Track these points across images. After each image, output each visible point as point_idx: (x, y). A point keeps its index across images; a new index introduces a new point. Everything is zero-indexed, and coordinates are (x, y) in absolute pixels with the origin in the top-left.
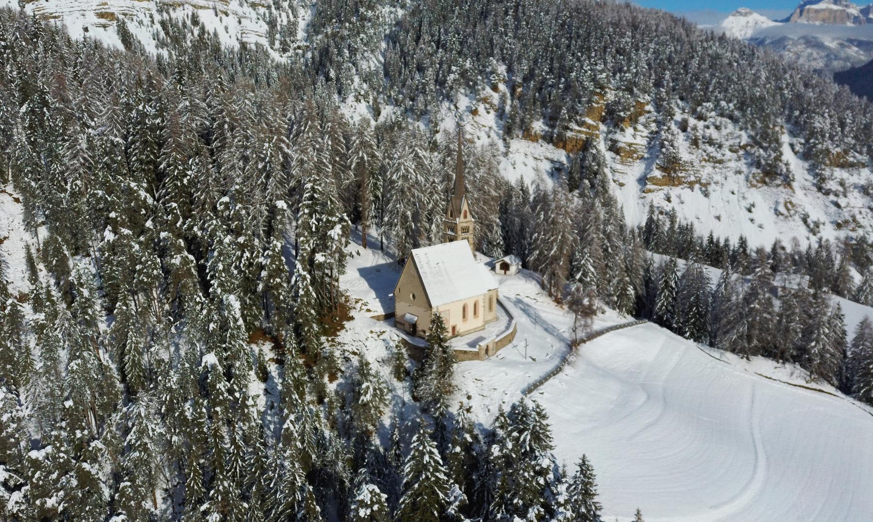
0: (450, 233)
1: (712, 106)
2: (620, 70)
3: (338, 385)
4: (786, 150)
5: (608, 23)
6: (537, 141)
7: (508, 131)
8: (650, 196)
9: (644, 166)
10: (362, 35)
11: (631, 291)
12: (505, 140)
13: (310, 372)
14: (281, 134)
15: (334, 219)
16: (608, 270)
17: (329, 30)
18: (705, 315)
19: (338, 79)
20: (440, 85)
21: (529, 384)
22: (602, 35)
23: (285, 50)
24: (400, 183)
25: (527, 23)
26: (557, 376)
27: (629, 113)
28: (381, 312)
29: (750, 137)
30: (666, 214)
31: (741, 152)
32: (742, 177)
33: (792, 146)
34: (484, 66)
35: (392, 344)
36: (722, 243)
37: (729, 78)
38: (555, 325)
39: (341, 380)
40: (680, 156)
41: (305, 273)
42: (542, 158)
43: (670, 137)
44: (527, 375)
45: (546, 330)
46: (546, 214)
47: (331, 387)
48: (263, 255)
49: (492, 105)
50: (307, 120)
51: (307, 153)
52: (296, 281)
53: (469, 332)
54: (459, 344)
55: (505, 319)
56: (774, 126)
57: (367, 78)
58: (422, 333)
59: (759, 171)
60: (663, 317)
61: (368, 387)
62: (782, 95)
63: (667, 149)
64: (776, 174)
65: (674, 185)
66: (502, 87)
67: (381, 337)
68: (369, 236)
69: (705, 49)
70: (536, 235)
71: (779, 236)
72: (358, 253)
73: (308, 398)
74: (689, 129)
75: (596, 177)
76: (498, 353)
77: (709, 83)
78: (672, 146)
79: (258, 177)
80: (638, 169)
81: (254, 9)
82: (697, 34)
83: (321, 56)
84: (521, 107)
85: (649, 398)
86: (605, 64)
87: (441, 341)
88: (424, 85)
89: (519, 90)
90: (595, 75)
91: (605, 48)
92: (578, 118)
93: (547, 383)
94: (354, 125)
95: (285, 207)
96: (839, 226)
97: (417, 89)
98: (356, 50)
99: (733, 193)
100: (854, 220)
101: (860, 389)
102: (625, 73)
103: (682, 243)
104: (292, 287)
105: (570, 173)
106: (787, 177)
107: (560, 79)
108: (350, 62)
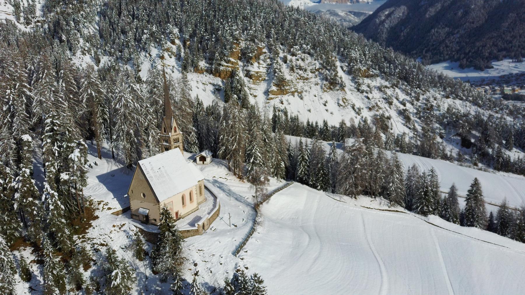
0: (165, 144)
2: (246, 29)
3: (92, 272)
4: (339, 69)
6: (203, 73)
7: (185, 68)
10: (82, 12)
13: (67, 266)
14: (23, 81)
15: (73, 145)
17: (59, 10)
18: (328, 174)
19: (68, 41)
20: (138, 42)
21: (236, 246)
22: (234, 9)
23: (28, 24)
24: (122, 110)
25: (188, 3)
27: (254, 54)
28: (119, 208)
31: (317, 73)
32: (319, 87)
33: (342, 67)
34: (164, 29)
35: (131, 233)
36: (314, 124)
38: (241, 195)
39: (94, 268)
41: (53, 192)
42: (207, 83)
44: (234, 239)
45: (236, 199)
47: (86, 275)
48: (14, 180)
49: (172, 53)
50: (44, 69)
51: (45, 95)
52: (46, 199)
55: (212, 198)
56: (332, 57)
57: (88, 39)
58: (154, 221)
59: (327, 83)
61: (117, 274)
62: (334, 40)
64: (336, 83)
65: (284, 94)
66: (177, 41)
67: (122, 229)
68: (103, 148)
69: (290, 16)
70: (222, 136)
71: (343, 118)
72: (96, 164)
73: (68, 287)
74: (288, 62)
75: (240, 93)
78: (280, 71)
79: (4, 117)
80: (263, 86)
82: (285, 7)
83: (55, 26)
85: (310, 238)
86: (237, 25)
88: (127, 42)
89: (188, 43)
90: (232, 33)
91: (236, 16)
94: (83, 70)
95: (30, 139)
96: (370, 109)
97: (123, 45)
98: (79, 22)
99: (315, 96)
100: (377, 106)
101: (417, 207)
102: (249, 31)
103: (295, 128)
104: (43, 203)
105: (226, 91)
106: (342, 85)
107: (212, 36)
108: (76, 30)
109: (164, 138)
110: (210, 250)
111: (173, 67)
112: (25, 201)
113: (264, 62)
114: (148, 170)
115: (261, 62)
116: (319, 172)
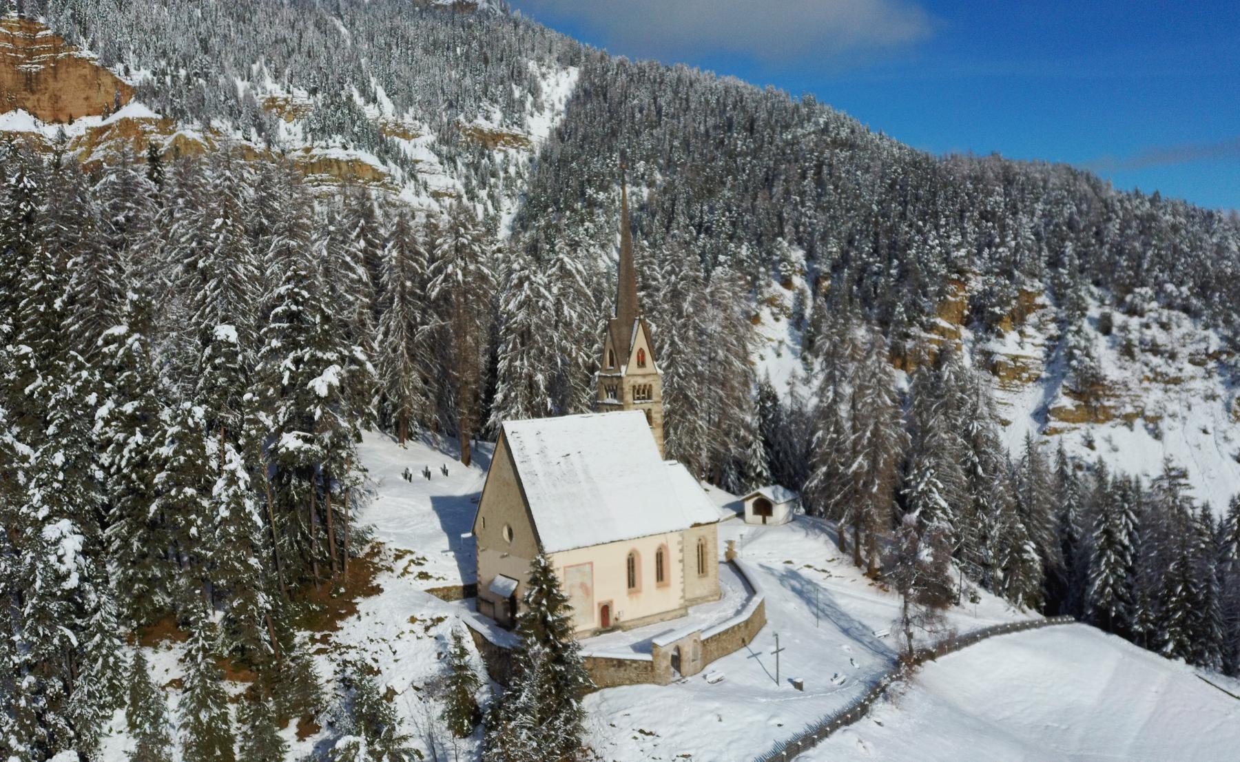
1: (1150, 292)
5: (964, 178)
10: (587, 224)
12: (804, 359)
16: (980, 514)
18: (1208, 600)
21: (777, 744)
22: (956, 194)
27: (1009, 308)
28: (454, 578)
29: (1223, 338)
31: (1212, 365)
32: (1218, 406)
37: (1175, 247)
38: (866, 622)
40: (1103, 373)
43: (1083, 343)
44: (776, 721)
45: (846, 631)
49: (782, 308)
60: (1108, 611)
63: (1080, 362)
65: (1097, 421)
66: (798, 281)
67: (433, 631)
72: (445, 472)
74: (1114, 331)
76: (710, 667)
77: (1141, 257)
78: (1088, 355)
81: (437, 201)
84: (830, 308)
86: (964, 235)
89: (826, 283)
90: (948, 253)
91: (962, 211)
92: (924, 319)
93: (827, 742)
99: (1205, 432)
102: (998, 246)
107: (890, 261)
109: (607, 382)
110: (678, 739)
111: (781, 342)
112: (173, 493)
113: (1039, 329)
114: (526, 452)
116: (1171, 591)
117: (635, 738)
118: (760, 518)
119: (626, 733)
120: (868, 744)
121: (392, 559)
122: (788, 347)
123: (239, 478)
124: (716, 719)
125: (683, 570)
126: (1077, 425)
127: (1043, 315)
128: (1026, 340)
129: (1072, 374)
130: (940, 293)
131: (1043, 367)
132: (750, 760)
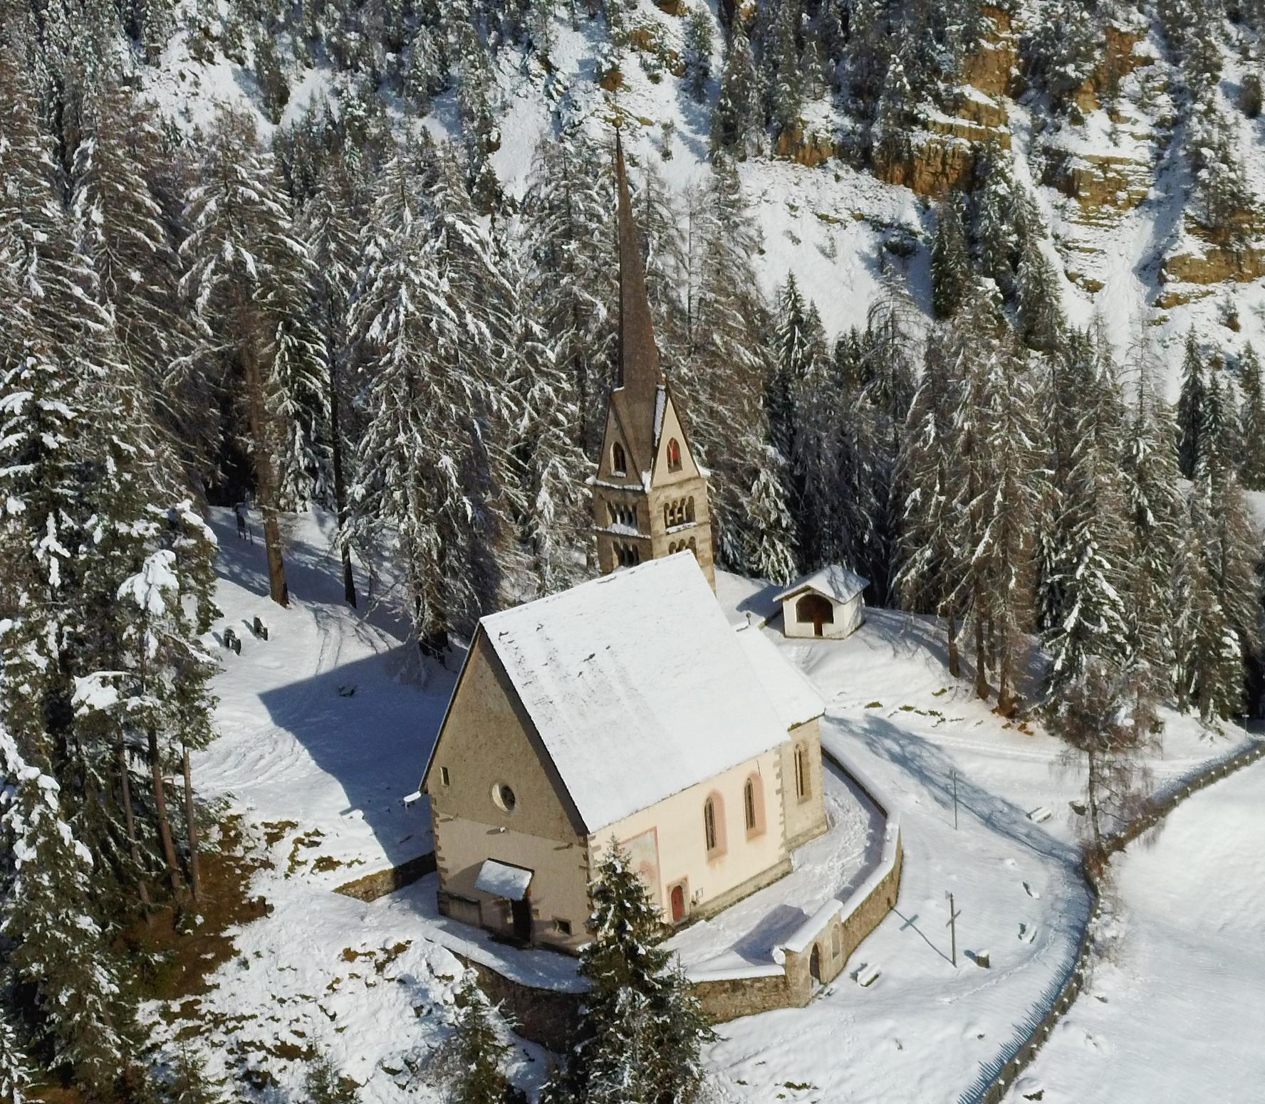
0: (619, 528)
6: (823, 164)
7: (727, 135)
8: (1181, 319)
9: (1150, 225)
11: (1232, 644)
12: (717, 162)
21: (986, 1068)
24: (399, 352)
26: (1073, 1011)
27: (1089, 67)
28: (376, 859)
30: (1230, 366)
35: (440, 993)
38: (1011, 798)
42: (845, 215)
44: (975, 1031)
46: (944, 422)
49: (664, 55)
53: (737, 898)
54: (708, 951)
55: (857, 818)
58: (556, 933)
63: (1213, 172)
65: (1241, 278)
67: (393, 970)
68: (299, 547)
70: (916, 493)
72: (258, 630)
75: (1016, 270)
78: (1225, 159)
80: (1133, 236)
84: (758, 58)
87: (637, 968)
92: (942, 86)
105: (939, 259)
109: (616, 498)
110: (847, 1088)
111: (668, 128)
114: (528, 666)
115: (1126, 108)
117: (781, 1096)
118: (811, 626)
119: (766, 1090)
120: (1099, 1038)
121: (263, 844)
122: (682, 137)
123: (44, 790)
124: (894, 1046)
125: (782, 804)
126: (1210, 287)
127: (1148, 78)
128: (1120, 127)
129: (1199, 194)
130: (970, 35)
131: (1150, 180)
132: (955, 1099)
